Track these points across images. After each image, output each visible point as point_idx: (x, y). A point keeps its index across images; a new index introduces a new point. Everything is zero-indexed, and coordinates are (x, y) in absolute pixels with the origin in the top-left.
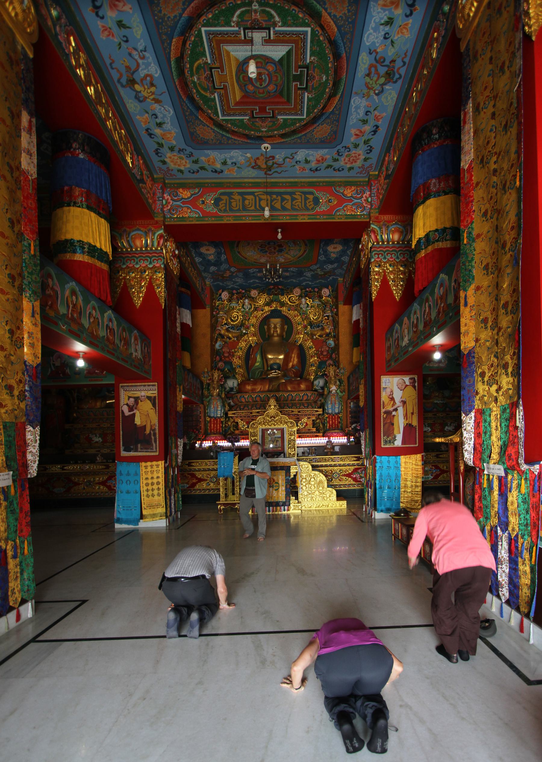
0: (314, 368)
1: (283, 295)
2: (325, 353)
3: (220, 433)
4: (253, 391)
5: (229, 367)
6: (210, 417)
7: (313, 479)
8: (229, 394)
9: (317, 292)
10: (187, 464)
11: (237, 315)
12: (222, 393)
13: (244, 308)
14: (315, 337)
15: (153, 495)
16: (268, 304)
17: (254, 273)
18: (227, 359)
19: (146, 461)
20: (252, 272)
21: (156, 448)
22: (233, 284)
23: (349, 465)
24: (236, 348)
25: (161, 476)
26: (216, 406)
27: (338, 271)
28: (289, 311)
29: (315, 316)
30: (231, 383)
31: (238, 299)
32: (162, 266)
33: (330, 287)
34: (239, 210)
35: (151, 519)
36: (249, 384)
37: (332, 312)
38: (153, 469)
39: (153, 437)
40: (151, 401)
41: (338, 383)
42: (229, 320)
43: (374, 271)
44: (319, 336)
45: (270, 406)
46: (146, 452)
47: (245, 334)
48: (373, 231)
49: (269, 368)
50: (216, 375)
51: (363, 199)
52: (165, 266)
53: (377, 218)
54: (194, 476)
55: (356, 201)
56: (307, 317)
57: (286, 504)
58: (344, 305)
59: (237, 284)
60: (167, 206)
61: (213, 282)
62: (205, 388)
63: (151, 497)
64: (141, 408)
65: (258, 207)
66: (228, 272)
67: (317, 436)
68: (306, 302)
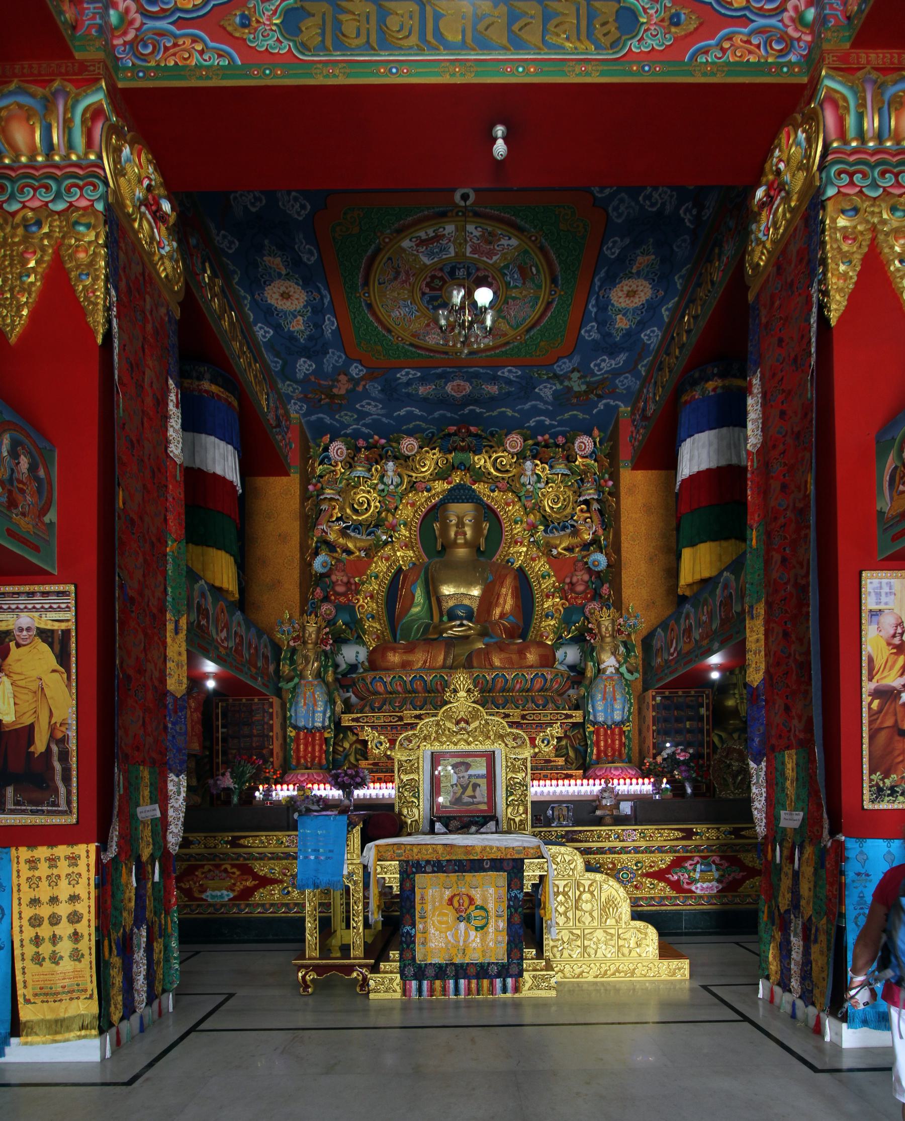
0: (552, 622)
1: (477, 452)
2: (580, 588)
3: (321, 767)
4: (405, 665)
5: (347, 618)
6: (295, 727)
7: (586, 896)
8: (346, 679)
9: (563, 447)
10: (227, 842)
11: (367, 498)
12: (326, 672)
13: (385, 484)
14: (555, 552)
15: (55, 959)
16: (442, 475)
17: (408, 384)
18: (343, 599)
19: (32, 844)
20: (404, 379)
21: (69, 802)
22: (357, 421)
23: (660, 850)
24: (365, 574)
25: (84, 895)
26: (310, 701)
27: (627, 382)
28: (493, 491)
29: (556, 503)
30: (351, 654)
31: (370, 462)
32: (100, 207)
33: (596, 432)
34: (368, 47)
35: (49, 1037)
36: (394, 650)
37: (599, 490)
38: (55, 871)
39: (57, 766)
40: (51, 645)
41: (622, 649)
42: (348, 511)
43: (835, 229)
44: (564, 549)
45: (455, 691)
46: (33, 812)
47: (386, 543)
48: (832, 99)
49: (445, 618)
50: (311, 628)
51: (786, 15)
52: (108, 207)
53: (844, 58)
54: (247, 871)
55: (761, 22)
56: (536, 504)
57: (510, 970)
58: (635, 468)
59: (368, 420)
60: (125, 33)
61: (307, 414)
62: (285, 658)
63: (47, 963)
64: (16, 667)
65: (430, 37)
66: (343, 378)
67: (568, 777)
68: (533, 470)
